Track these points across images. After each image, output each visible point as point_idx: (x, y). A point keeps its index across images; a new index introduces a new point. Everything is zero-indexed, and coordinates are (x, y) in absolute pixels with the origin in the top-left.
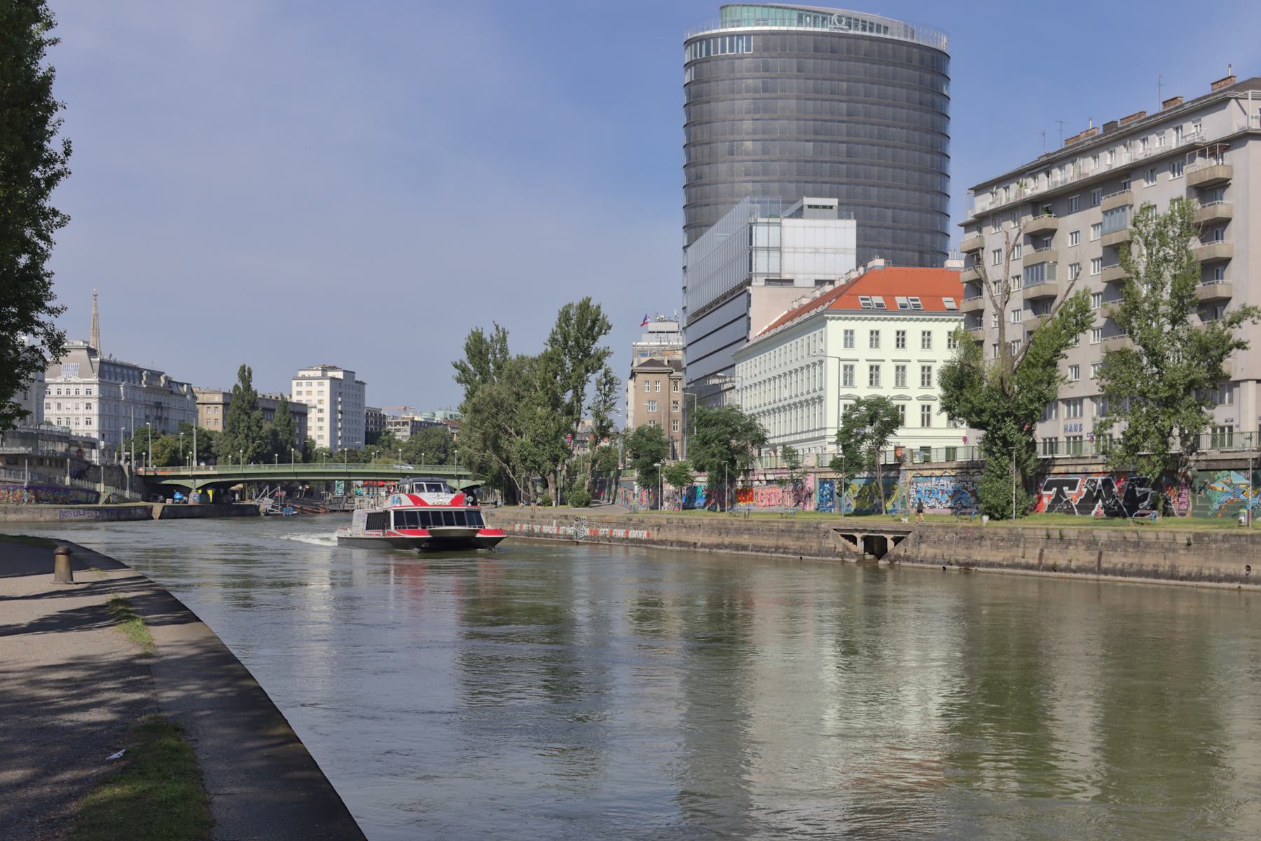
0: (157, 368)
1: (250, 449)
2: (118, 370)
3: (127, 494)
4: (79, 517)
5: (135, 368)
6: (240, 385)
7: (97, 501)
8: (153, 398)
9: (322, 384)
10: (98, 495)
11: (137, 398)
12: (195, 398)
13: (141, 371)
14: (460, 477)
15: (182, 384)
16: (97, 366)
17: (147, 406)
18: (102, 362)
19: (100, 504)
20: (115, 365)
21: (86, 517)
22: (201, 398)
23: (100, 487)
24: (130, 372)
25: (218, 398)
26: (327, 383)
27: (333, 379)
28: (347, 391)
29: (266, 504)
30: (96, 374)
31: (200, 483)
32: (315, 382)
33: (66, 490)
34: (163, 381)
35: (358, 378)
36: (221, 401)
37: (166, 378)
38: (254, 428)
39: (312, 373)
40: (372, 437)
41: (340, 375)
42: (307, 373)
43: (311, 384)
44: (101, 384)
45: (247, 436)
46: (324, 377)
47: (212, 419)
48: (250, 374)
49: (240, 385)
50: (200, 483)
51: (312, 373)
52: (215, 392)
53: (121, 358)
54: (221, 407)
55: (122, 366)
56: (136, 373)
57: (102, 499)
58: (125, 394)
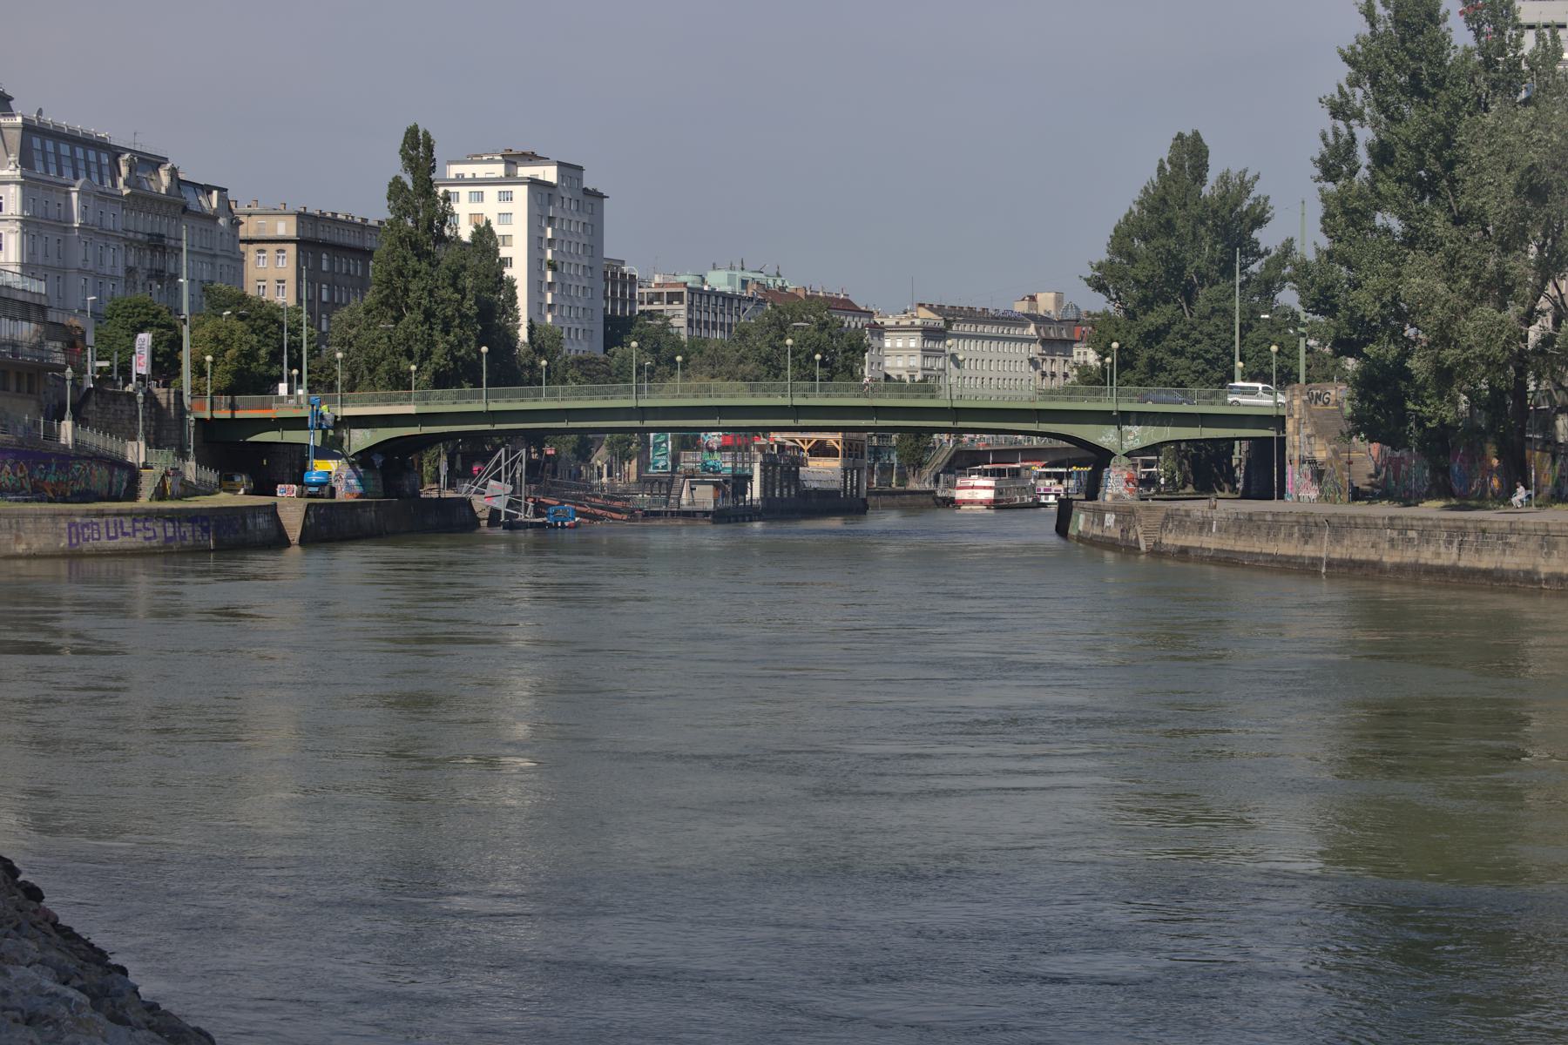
0: (151, 147)
1: (441, 347)
2: (65, 149)
3: (191, 470)
4: (123, 542)
5: (100, 145)
6: (408, 179)
7: (132, 494)
8: (144, 224)
9: (506, 197)
10: (134, 474)
11: (109, 223)
12: (235, 224)
13: (115, 152)
14: (1124, 418)
15: (208, 189)
16: (14, 138)
17: (130, 243)
18: (28, 129)
19: (144, 501)
20: (57, 135)
21: (137, 541)
22: (249, 228)
23: (136, 451)
24: (94, 153)
25: (285, 227)
26: (521, 192)
27: (534, 183)
28: (568, 205)
29: (490, 496)
30: (13, 157)
31: (1137, 436)
32: (491, 192)
33: (64, 458)
34: (165, 177)
35: (588, 183)
36: (293, 233)
37: (173, 172)
38: (447, 293)
39: (481, 170)
40: (616, 329)
41: (549, 174)
42: (468, 170)
43: (480, 197)
44: (28, 185)
45: (429, 315)
46: (510, 179)
47: (272, 276)
48: (429, 148)
49: (408, 179)
50: (1137, 436)
51: (481, 170)
52: (275, 213)
53: (60, 117)
54: (291, 249)
55: (73, 139)
56: (105, 160)
57: (147, 485)
58: (83, 214)
